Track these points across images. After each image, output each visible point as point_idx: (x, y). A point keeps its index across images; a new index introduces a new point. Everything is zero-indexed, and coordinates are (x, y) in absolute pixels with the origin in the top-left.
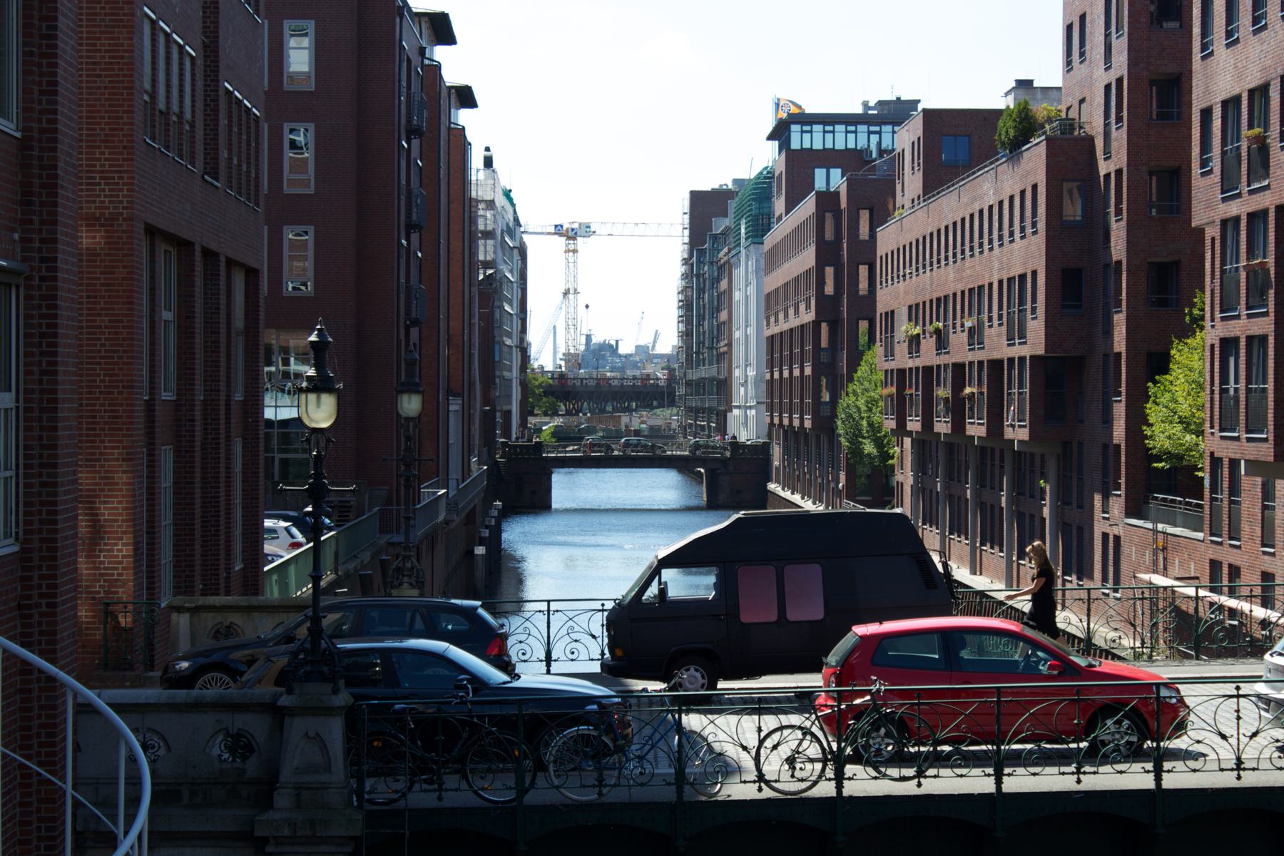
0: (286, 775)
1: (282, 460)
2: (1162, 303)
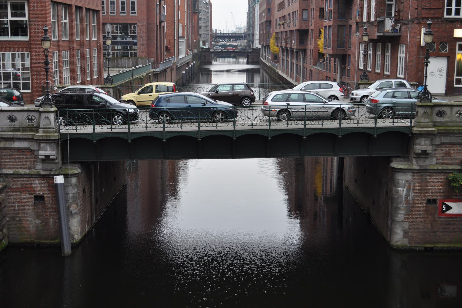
0: (41, 126)
1: (130, 52)
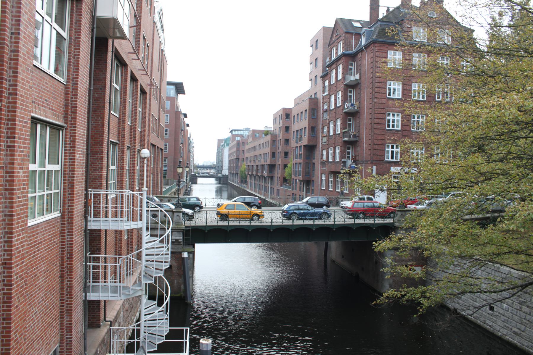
2: (286, 158)
